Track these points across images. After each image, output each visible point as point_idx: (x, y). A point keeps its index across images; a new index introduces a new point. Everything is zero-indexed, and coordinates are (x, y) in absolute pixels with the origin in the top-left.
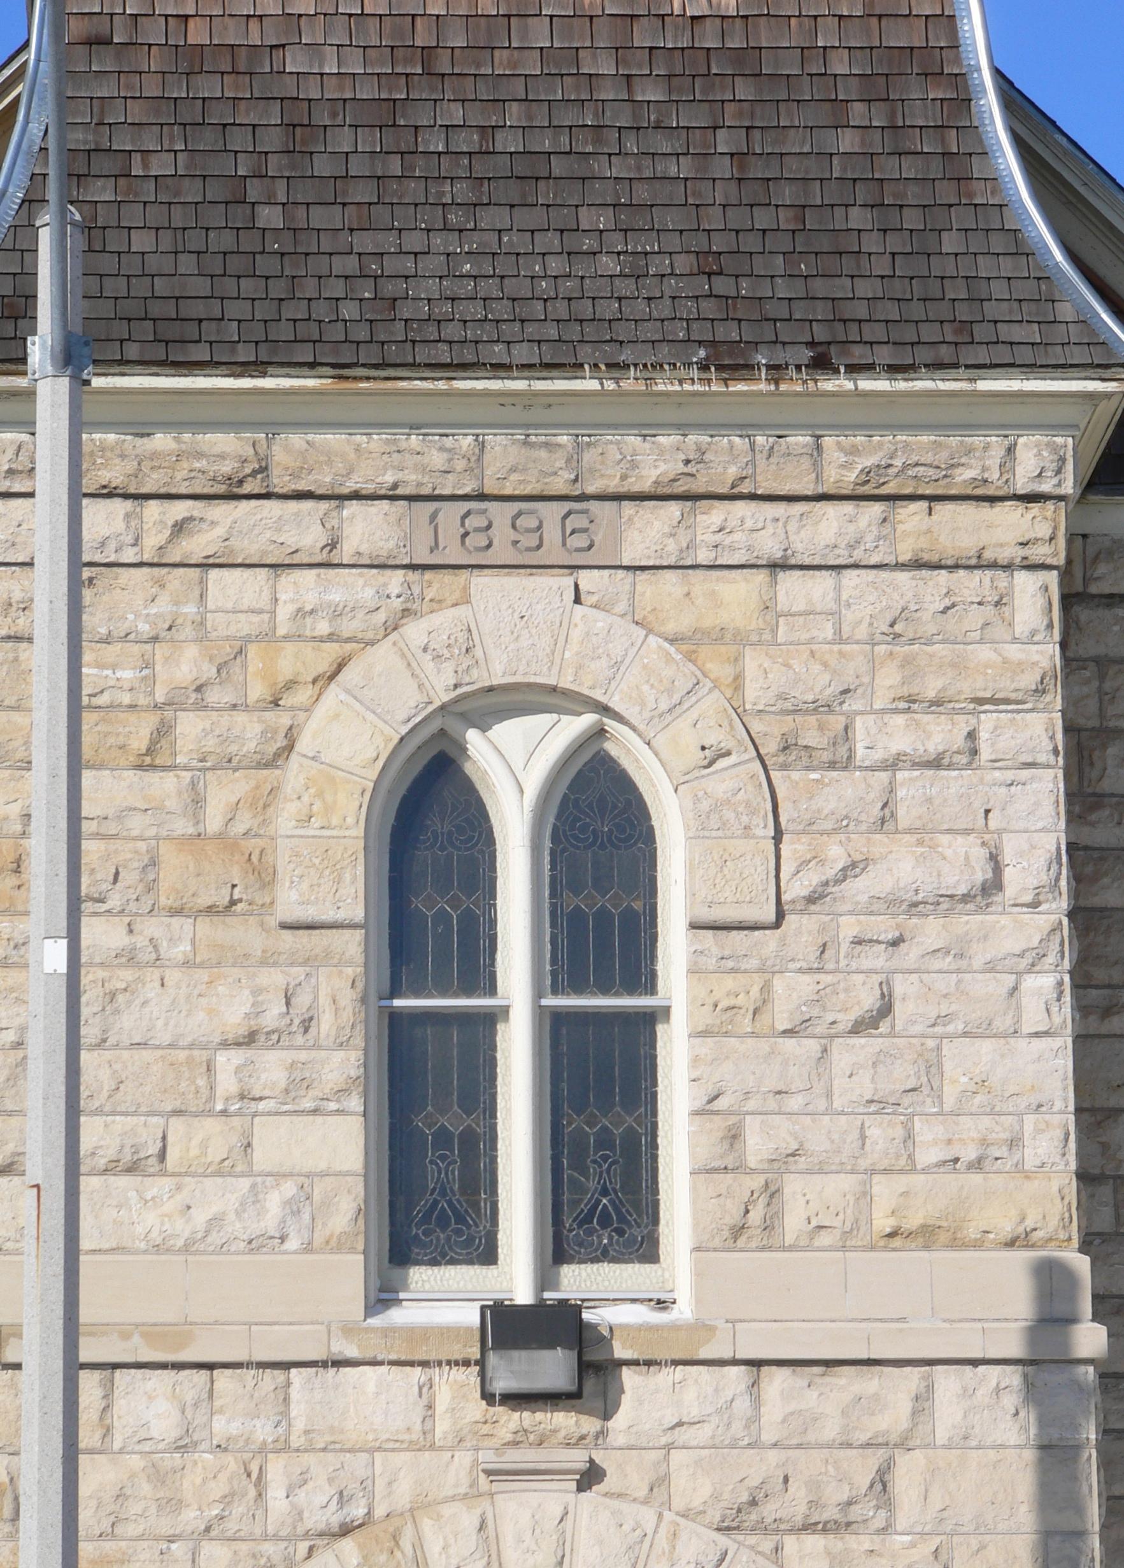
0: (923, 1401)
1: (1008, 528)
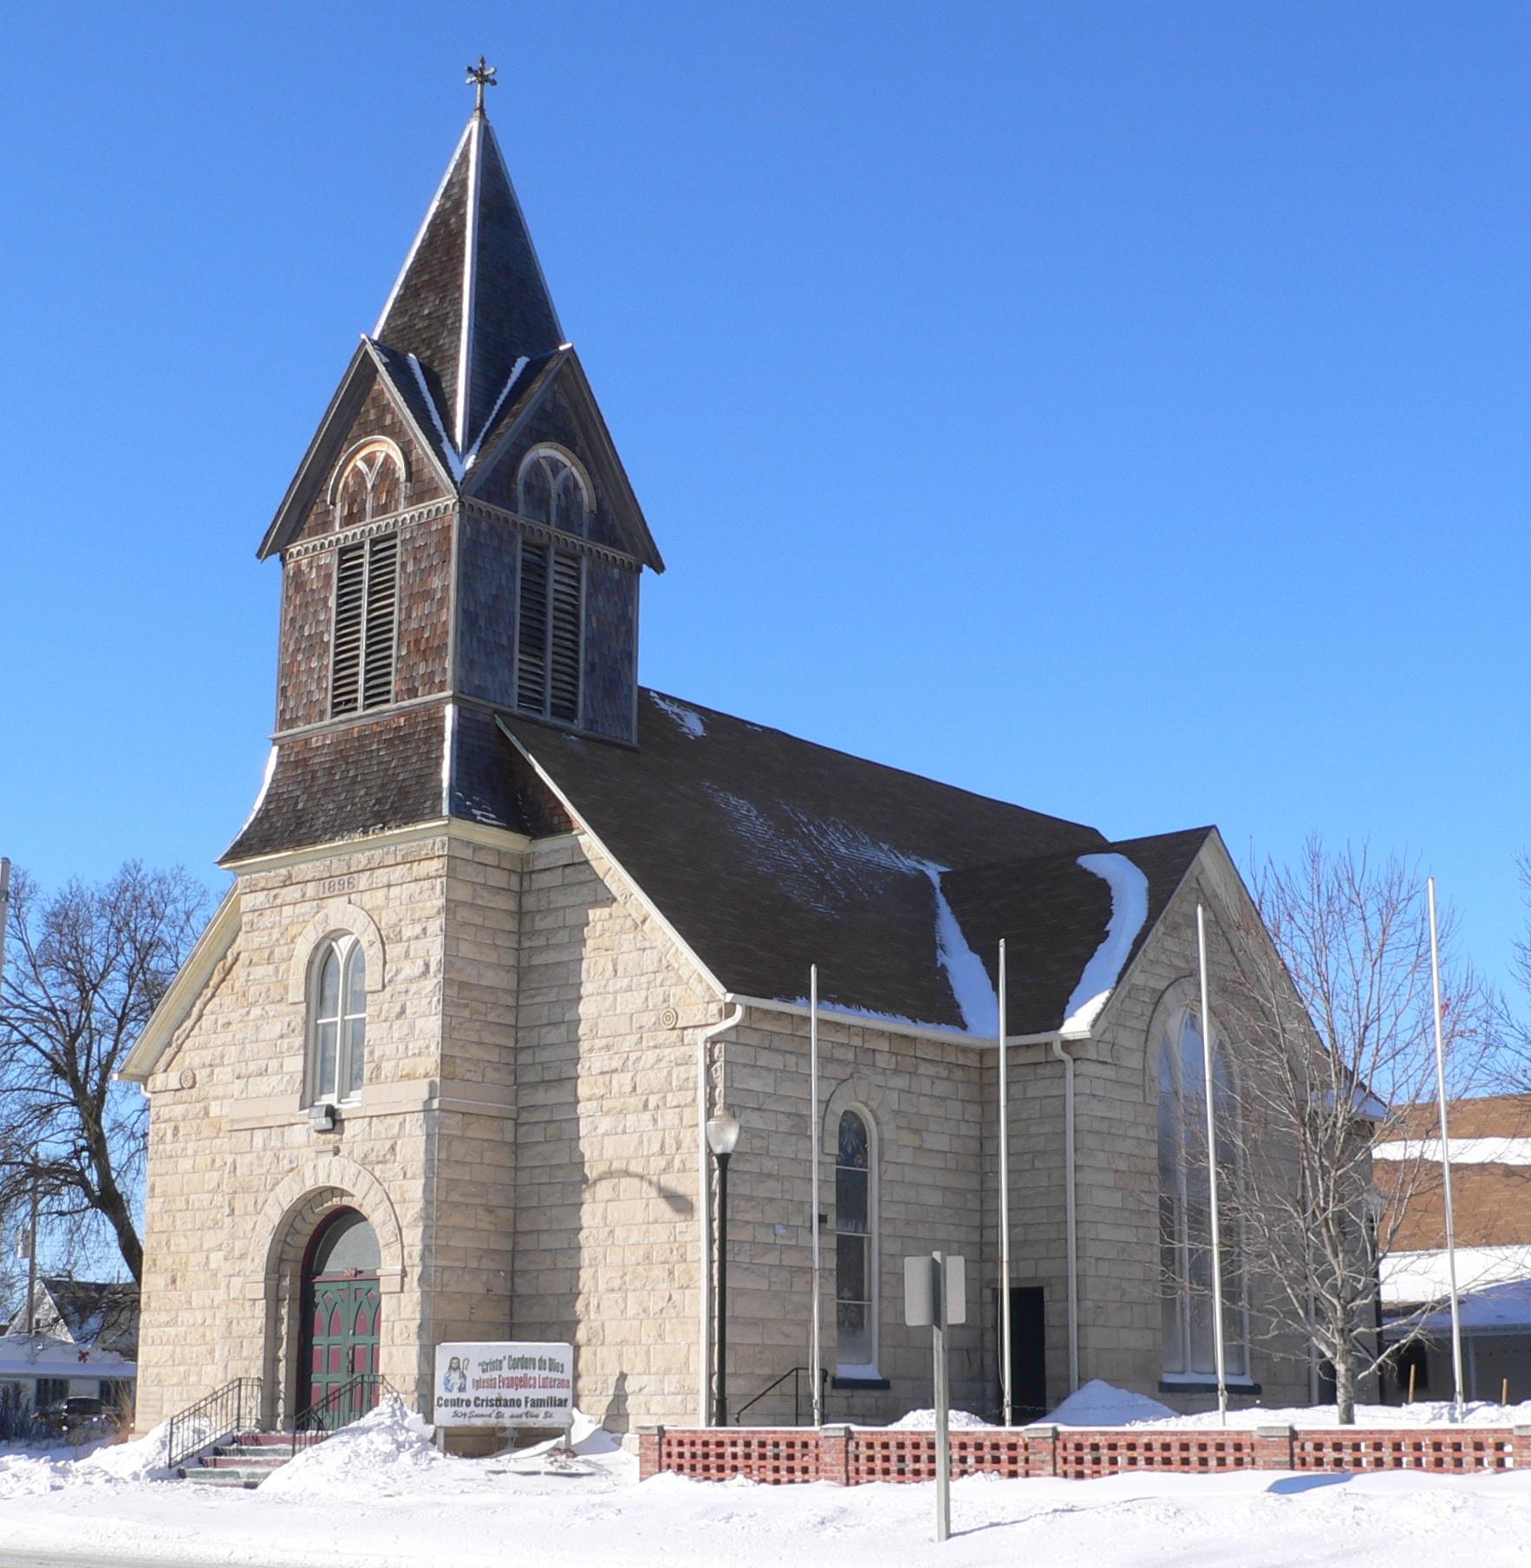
0: (402, 1125)
1: (435, 866)
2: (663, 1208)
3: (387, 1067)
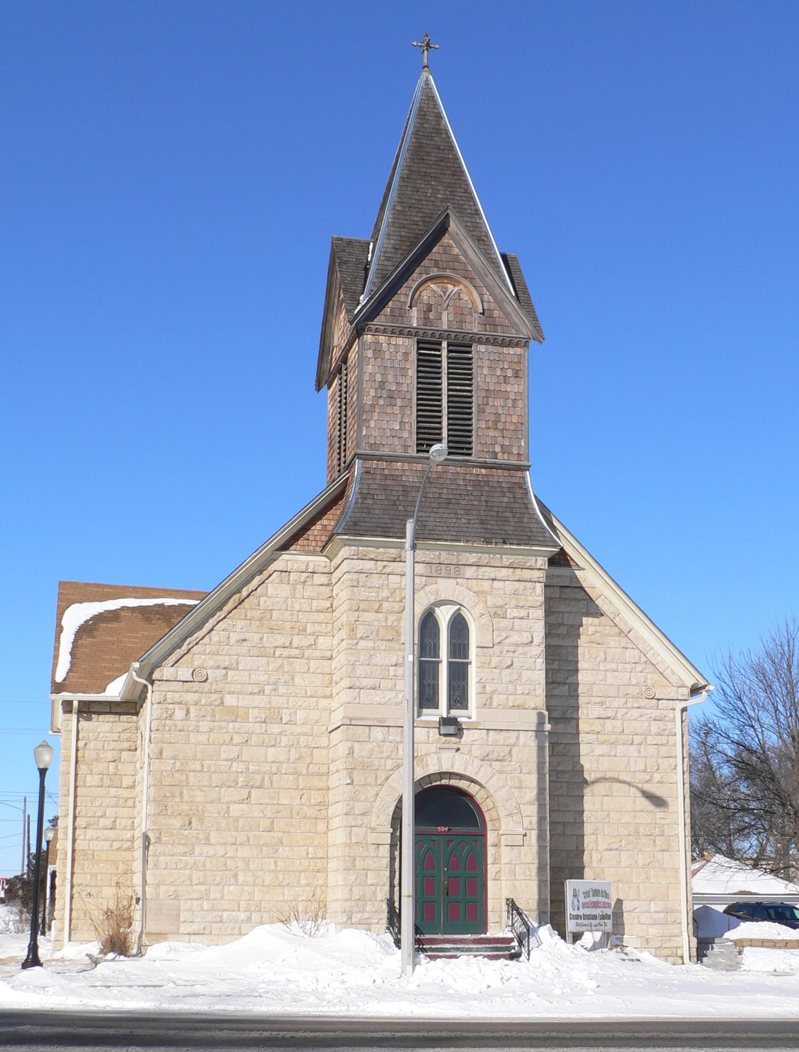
0: (518, 737)
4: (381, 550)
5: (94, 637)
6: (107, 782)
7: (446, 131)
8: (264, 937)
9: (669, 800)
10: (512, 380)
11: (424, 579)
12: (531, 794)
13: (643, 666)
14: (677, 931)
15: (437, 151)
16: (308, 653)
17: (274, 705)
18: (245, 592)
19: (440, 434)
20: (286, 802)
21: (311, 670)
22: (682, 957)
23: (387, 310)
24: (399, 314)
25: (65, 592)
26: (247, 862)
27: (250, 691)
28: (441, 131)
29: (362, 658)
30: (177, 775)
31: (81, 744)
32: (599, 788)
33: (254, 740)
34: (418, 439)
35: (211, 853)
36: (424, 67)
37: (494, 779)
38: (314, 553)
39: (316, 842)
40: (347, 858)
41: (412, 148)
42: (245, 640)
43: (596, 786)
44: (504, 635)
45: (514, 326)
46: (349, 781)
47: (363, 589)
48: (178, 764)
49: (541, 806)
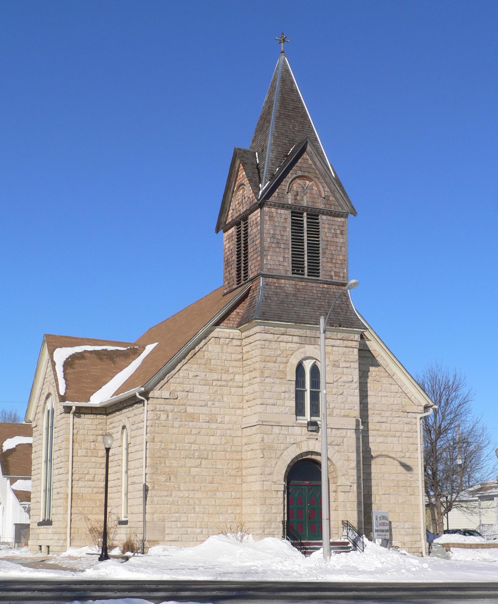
2: (401, 469)
3: (336, 412)
4: (276, 328)
5: (74, 368)
6: (90, 454)
7: (297, 90)
8: (215, 542)
9: (414, 467)
10: (340, 236)
11: (298, 345)
12: (354, 464)
13: (401, 394)
14: (419, 539)
15: (292, 102)
16: (230, 384)
17: (213, 412)
18: (197, 349)
19: (303, 264)
20: (220, 467)
21: (232, 394)
22: (422, 553)
23: (275, 194)
24: (282, 196)
25: (50, 341)
26: (199, 499)
27: (200, 404)
28: (293, 91)
29: (268, 388)
30: (163, 452)
31: (75, 431)
32: (379, 460)
33: (203, 432)
34: (292, 267)
35: (181, 495)
36: (282, 52)
37: (335, 456)
38: (232, 328)
39: (236, 489)
40: (262, 499)
41: (279, 100)
42: (197, 376)
43: (377, 459)
44: (339, 376)
45: (340, 205)
46: (262, 456)
47: (267, 350)
48: (163, 445)
49: (358, 470)
